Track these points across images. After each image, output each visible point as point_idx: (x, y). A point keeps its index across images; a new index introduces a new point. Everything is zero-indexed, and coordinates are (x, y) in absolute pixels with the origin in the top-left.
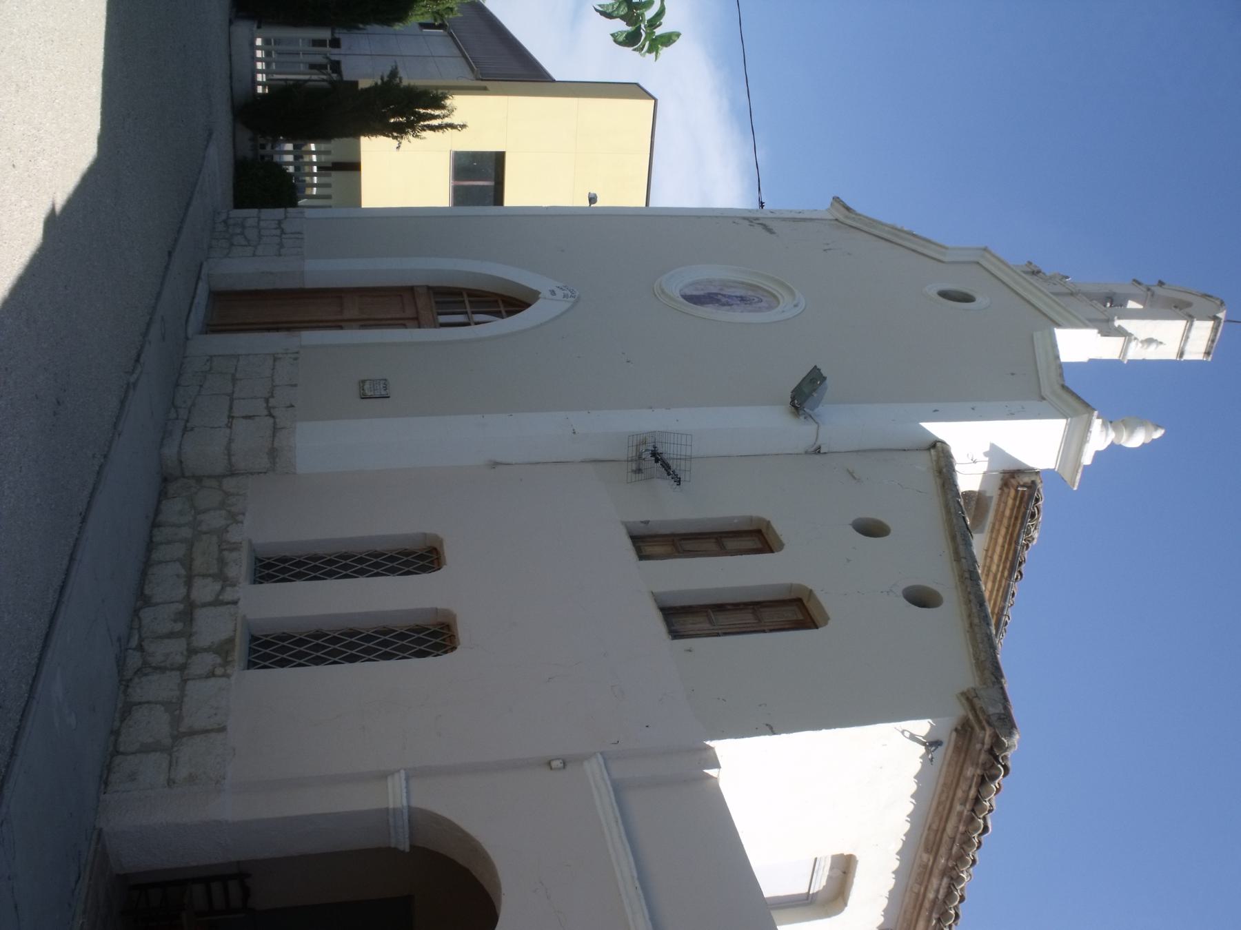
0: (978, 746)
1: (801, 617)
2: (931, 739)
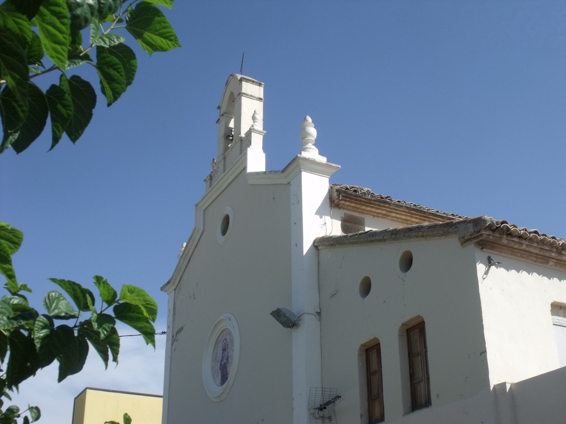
0: (491, 237)
1: (418, 330)
2: (487, 263)
